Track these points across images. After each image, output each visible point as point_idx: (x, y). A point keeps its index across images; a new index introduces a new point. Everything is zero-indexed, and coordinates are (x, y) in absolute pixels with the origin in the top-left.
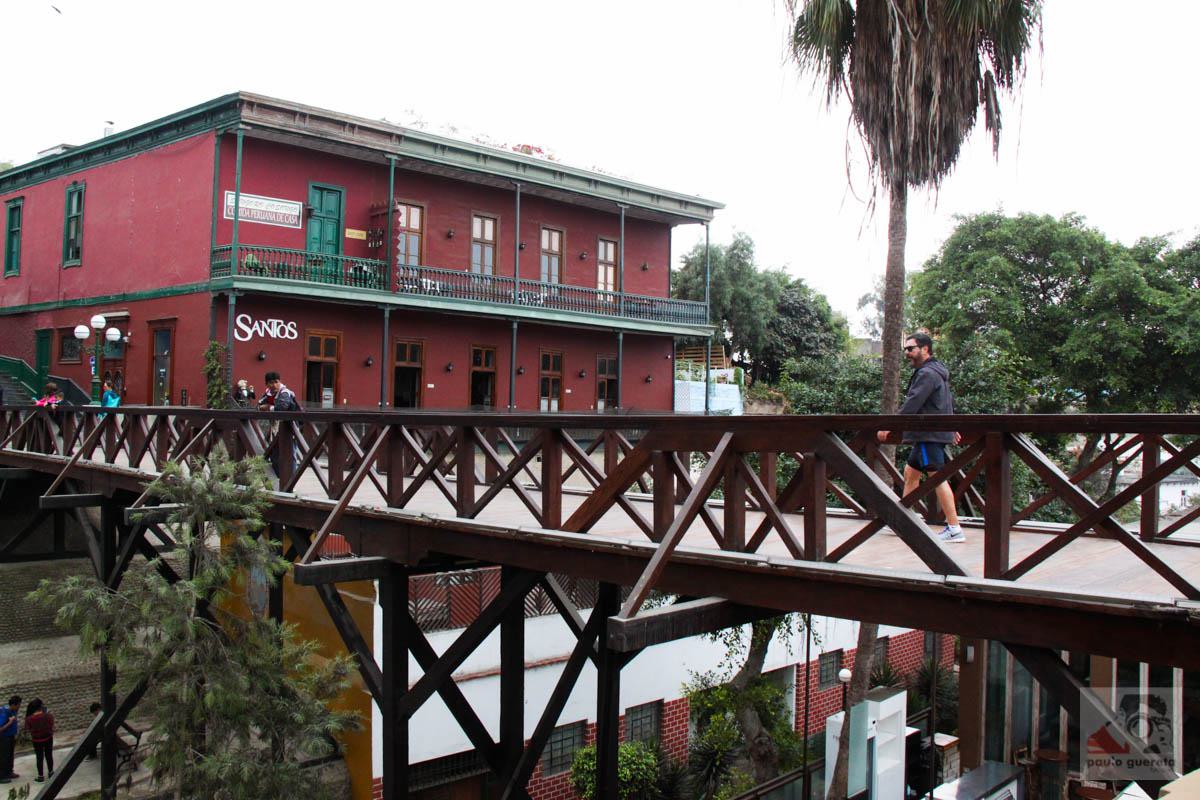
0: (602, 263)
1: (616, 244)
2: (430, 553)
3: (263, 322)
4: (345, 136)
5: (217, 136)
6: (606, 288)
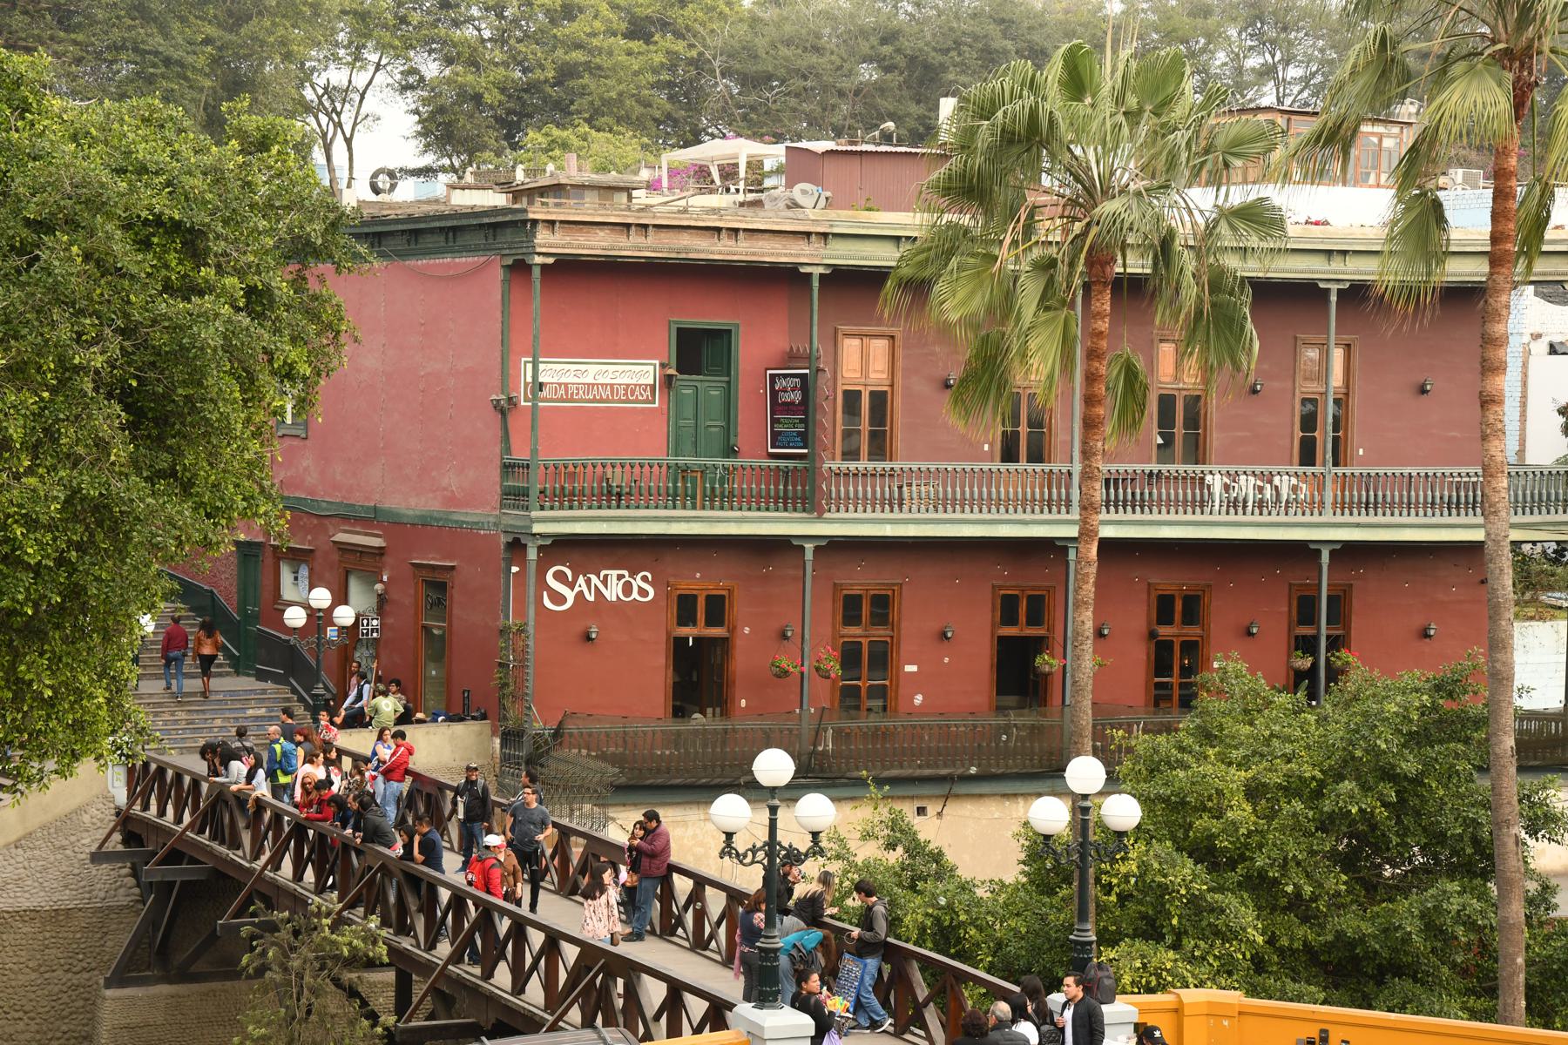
3: (594, 578)
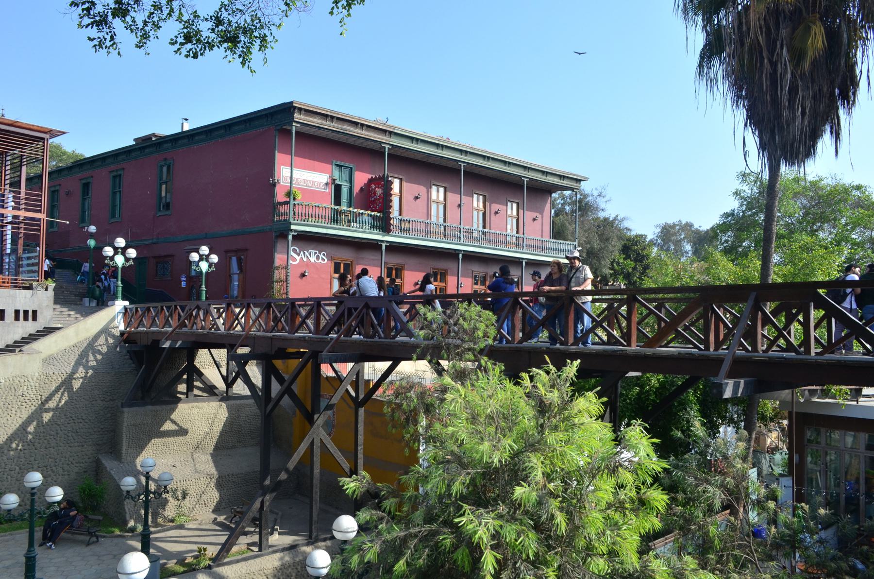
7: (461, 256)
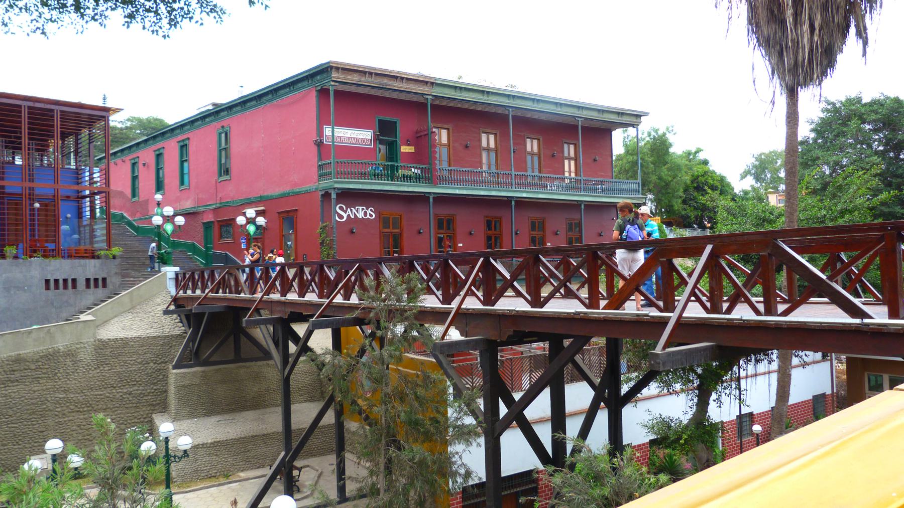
0: (566, 158)
1: (575, 145)
2: (514, 331)
4: (398, 85)
5: (316, 91)
6: (570, 175)
7: (513, 203)
